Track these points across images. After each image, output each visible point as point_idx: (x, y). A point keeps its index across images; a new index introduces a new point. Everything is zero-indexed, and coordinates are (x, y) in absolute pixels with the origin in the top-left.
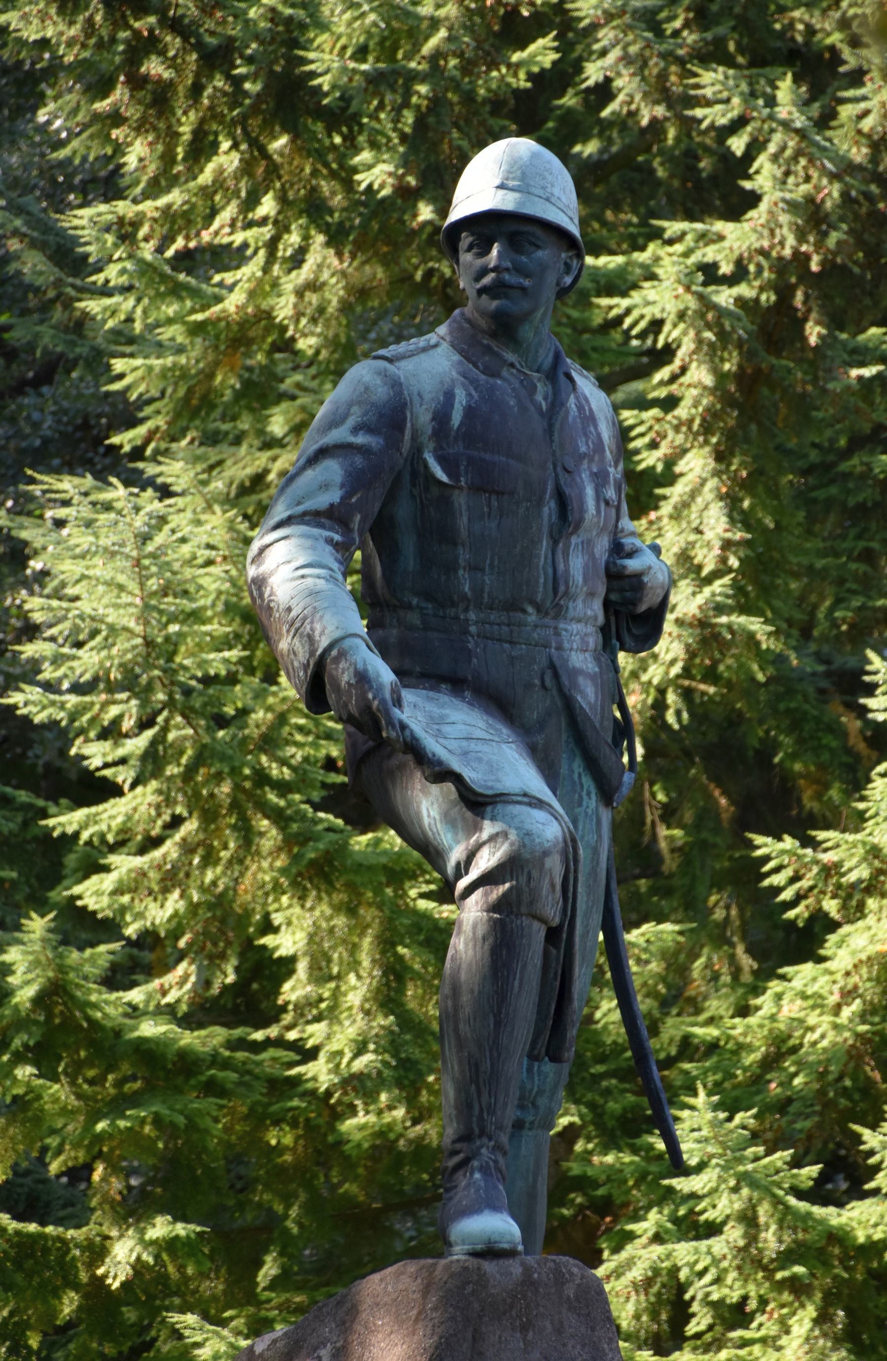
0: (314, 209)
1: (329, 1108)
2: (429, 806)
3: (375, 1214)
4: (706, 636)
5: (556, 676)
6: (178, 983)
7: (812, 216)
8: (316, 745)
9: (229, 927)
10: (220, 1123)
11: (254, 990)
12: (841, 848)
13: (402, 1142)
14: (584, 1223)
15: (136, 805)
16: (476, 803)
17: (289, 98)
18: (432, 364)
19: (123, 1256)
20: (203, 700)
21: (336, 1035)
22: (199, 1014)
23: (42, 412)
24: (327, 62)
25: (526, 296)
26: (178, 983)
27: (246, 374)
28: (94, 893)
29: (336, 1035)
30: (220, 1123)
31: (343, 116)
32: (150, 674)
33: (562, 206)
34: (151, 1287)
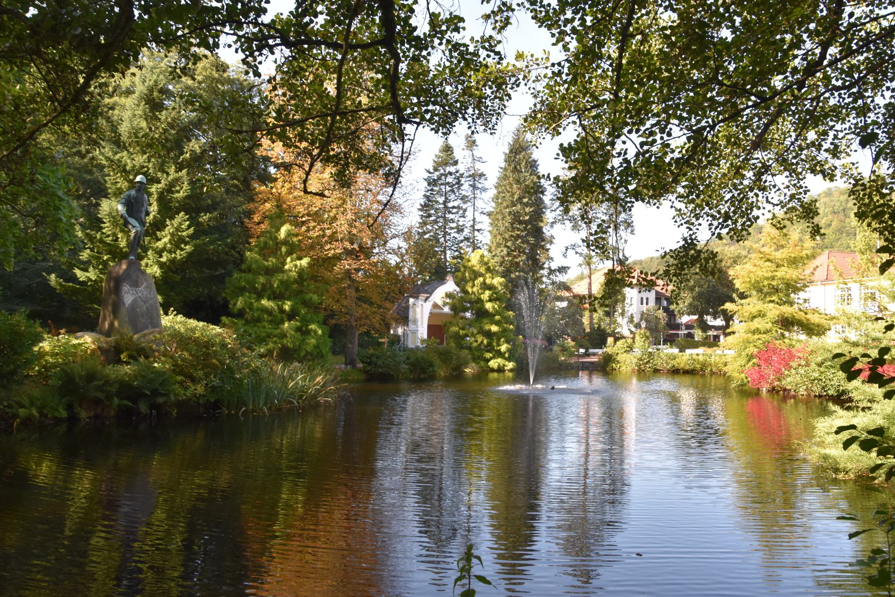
0: (126, 179)
1: (122, 249)
2: (130, 227)
3: (123, 256)
4: (155, 216)
5: (141, 218)
6: (110, 238)
7: (166, 185)
8: (122, 221)
9: (114, 234)
10: (113, 249)
11: (117, 239)
12: (163, 233)
13: (653, 159)
14: (140, 258)
15: (108, 224)
16: (134, 227)
17: (125, 170)
18: (133, 192)
19: (105, 258)
20: (114, 217)
21: (123, 243)
22: (112, 241)
23: (103, 194)
24: (128, 168)
25: (142, 188)
26: (110, 238)
27: (118, 193)
28: (104, 231)
29: (123, 243)
30: (113, 249)
31: (129, 172)
32: (110, 214)
33: (145, 181)
34: (107, 260)
